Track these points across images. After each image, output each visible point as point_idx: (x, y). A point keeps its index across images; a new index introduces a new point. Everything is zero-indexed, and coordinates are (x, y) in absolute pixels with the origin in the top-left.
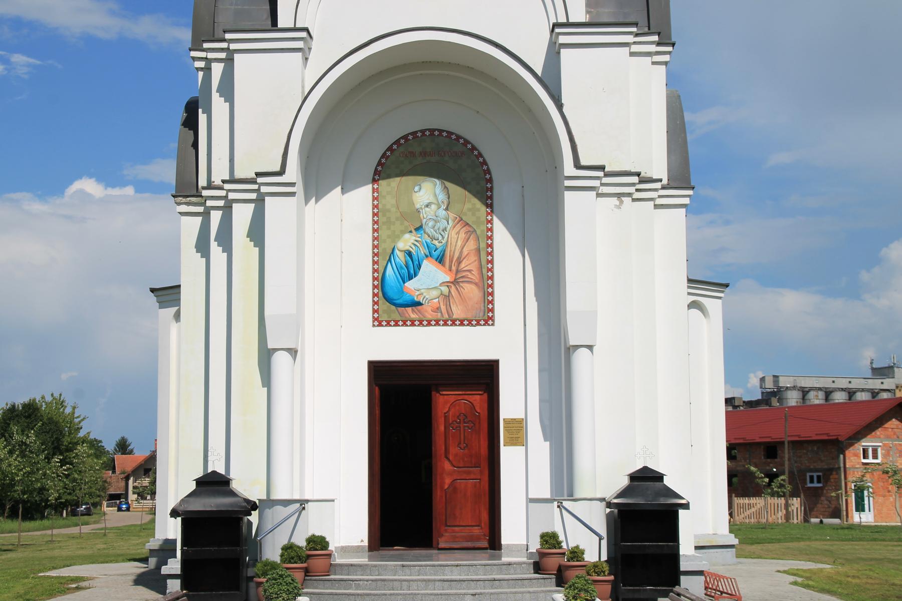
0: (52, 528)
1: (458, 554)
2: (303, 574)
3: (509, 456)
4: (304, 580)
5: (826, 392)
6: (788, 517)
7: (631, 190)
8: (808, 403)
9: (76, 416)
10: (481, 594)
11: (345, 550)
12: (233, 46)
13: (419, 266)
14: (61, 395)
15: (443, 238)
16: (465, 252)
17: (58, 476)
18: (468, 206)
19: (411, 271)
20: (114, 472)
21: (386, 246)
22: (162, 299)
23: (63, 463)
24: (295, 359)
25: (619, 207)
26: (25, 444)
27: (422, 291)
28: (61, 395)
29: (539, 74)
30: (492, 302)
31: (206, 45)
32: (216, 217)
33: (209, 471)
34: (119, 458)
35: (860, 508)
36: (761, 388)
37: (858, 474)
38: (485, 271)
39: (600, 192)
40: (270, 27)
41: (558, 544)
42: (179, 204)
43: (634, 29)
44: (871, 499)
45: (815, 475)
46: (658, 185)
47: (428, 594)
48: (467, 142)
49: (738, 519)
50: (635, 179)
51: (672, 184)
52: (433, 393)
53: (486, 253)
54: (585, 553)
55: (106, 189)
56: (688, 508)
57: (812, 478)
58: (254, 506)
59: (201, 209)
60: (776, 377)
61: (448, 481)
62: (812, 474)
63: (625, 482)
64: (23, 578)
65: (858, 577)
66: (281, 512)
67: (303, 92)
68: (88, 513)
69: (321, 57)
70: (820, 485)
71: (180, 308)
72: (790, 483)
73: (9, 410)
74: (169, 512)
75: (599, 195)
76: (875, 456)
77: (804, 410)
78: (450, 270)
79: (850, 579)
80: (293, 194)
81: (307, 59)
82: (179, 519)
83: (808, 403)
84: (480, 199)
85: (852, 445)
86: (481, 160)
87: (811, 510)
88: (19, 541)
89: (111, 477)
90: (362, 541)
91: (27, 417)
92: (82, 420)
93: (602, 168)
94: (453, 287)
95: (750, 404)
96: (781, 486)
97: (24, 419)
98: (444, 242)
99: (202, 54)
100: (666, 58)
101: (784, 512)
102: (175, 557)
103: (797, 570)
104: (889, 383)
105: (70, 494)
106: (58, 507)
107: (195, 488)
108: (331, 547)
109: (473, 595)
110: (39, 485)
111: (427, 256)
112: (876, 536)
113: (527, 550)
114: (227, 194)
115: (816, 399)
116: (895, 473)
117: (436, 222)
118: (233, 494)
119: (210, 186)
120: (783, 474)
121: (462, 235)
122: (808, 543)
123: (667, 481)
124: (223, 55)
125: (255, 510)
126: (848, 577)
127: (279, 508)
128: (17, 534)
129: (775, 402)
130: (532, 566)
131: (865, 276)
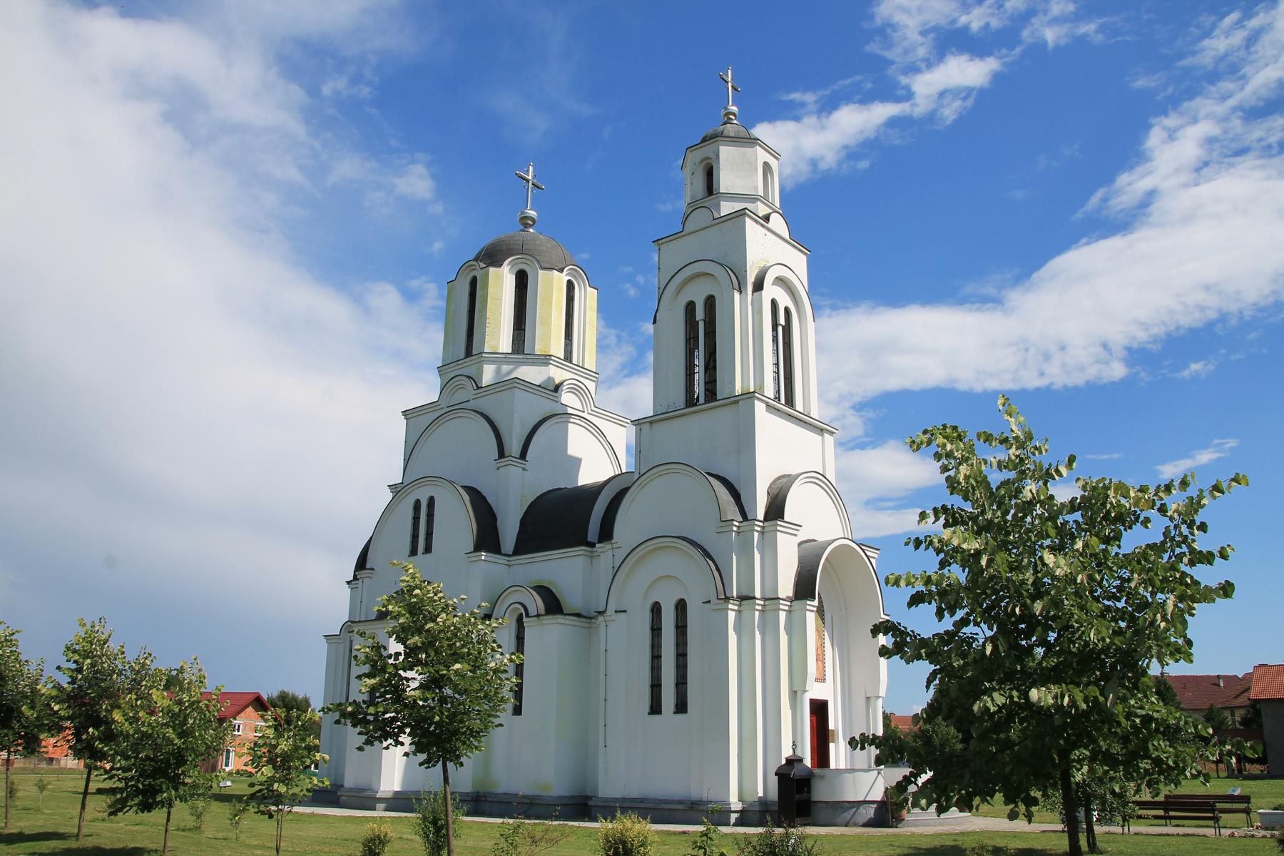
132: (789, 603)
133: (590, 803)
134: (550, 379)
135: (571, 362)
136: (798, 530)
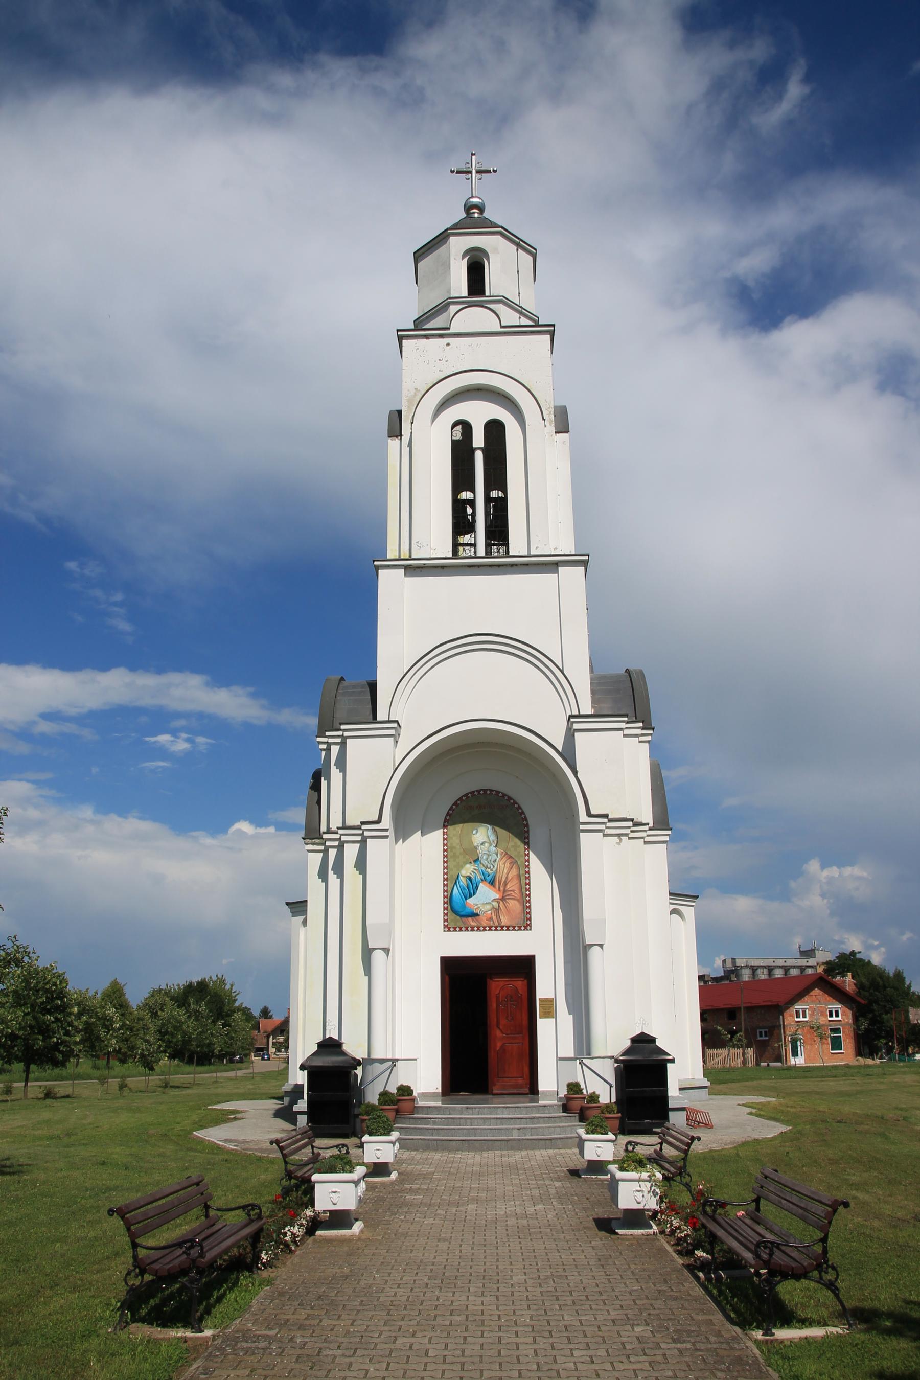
0: (217, 1072)
1: (507, 1098)
2: (395, 1113)
3: (544, 1026)
4: (396, 1118)
5: (769, 969)
6: (744, 1062)
7: (627, 831)
8: (757, 978)
9: (233, 991)
10: (524, 1128)
11: (425, 1095)
12: (346, 734)
13: (477, 888)
14: (223, 976)
15: (494, 867)
16: (510, 877)
17: (221, 1035)
18: (511, 844)
19: (471, 890)
20: (259, 1031)
21: (453, 873)
22: (294, 910)
23: (224, 1025)
24: (388, 956)
25: (619, 844)
26: (198, 1011)
27: (479, 905)
28: (223, 976)
29: (560, 750)
30: (529, 913)
31: (327, 734)
32: (332, 853)
33: (327, 1037)
34: (262, 1022)
35: (795, 1054)
36: (723, 967)
37: (793, 1030)
38: (524, 890)
39: (605, 833)
40: (371, 720)
41: (580, 1091)
42: (307, 844)
43: (626, 719)
44: (802, 1047)
45: (763, 1031)
46: (646, 828)
47: (485, 1129)
48: (510, 798)
49: (710, 1065)
50: (630, 824)
51: (656, 827)
52: (488, 980)
53: (524, 878)
54: (600, 1097)
55: (256, 828)
56: (674, 1062)
57: (761, 1033)
58: (358, 1063)
59: (322, 848)
60: (733, 959)
61: (499, 1045)
62: (760, 1030)
63: (628, 1044)
64: (197, 1109)
65: (795, 1107)
66: (379, 1068)
67: (394, 765)
68: (241, 1061)
69: (406, 742)
70: (767, 1038)
71: (306, 917)
72: (745, 1038)
73: (188, 986)
74: (299, 1066)
75: (604, 835)
76: (804, 1016)
77: (755, 983)
78: (499, 890)
79: (789, 1109)
80: (387, 837)
81: (397, 742)
82: (306, 1072)
83: (757, 978)
84: (520, 839)
85: (788, 1008)
86: (520, 811)
87: (761, 1057)
88: (194, 1081)
89: (257, 1035)
90: (437, 1089)
91: (199, 992)
92: (238, 994)
93: (606, 816)
94: (501, 902)
95: (716, 979)
96: (740, 1040)
97: (198, 993)
98: (494, 870)
99: (325, 740)
100: (649, 738)
101: (742, 1058)
102: (303, 1099)
103: (752, 1103)
104: (812, 962)
105: (228, 1047)
106: (221, 1057)
107: (317, 1049)
108: (415, 1094)
109: (518, 1129)
110: (208, 1041)
111: (482, 880)
112: (807, 1074)
113: (557, 1095)
114: (340, 837)
115: (762, 975)
116: (818, 1028)
117: (489, 855)
118: (344, 1054)
119: (329, 831)
120: (741, 1031)
121: (508, 865)
122: (759, 1082)
123: (658, 1043)
124: (339, 740)
125: (360, 1066)
126: (788, 1107)
127: (377, 1065)
128: (192, 1076)
129: (733, 978)
130: (561, 1107)
131: (793, 884)
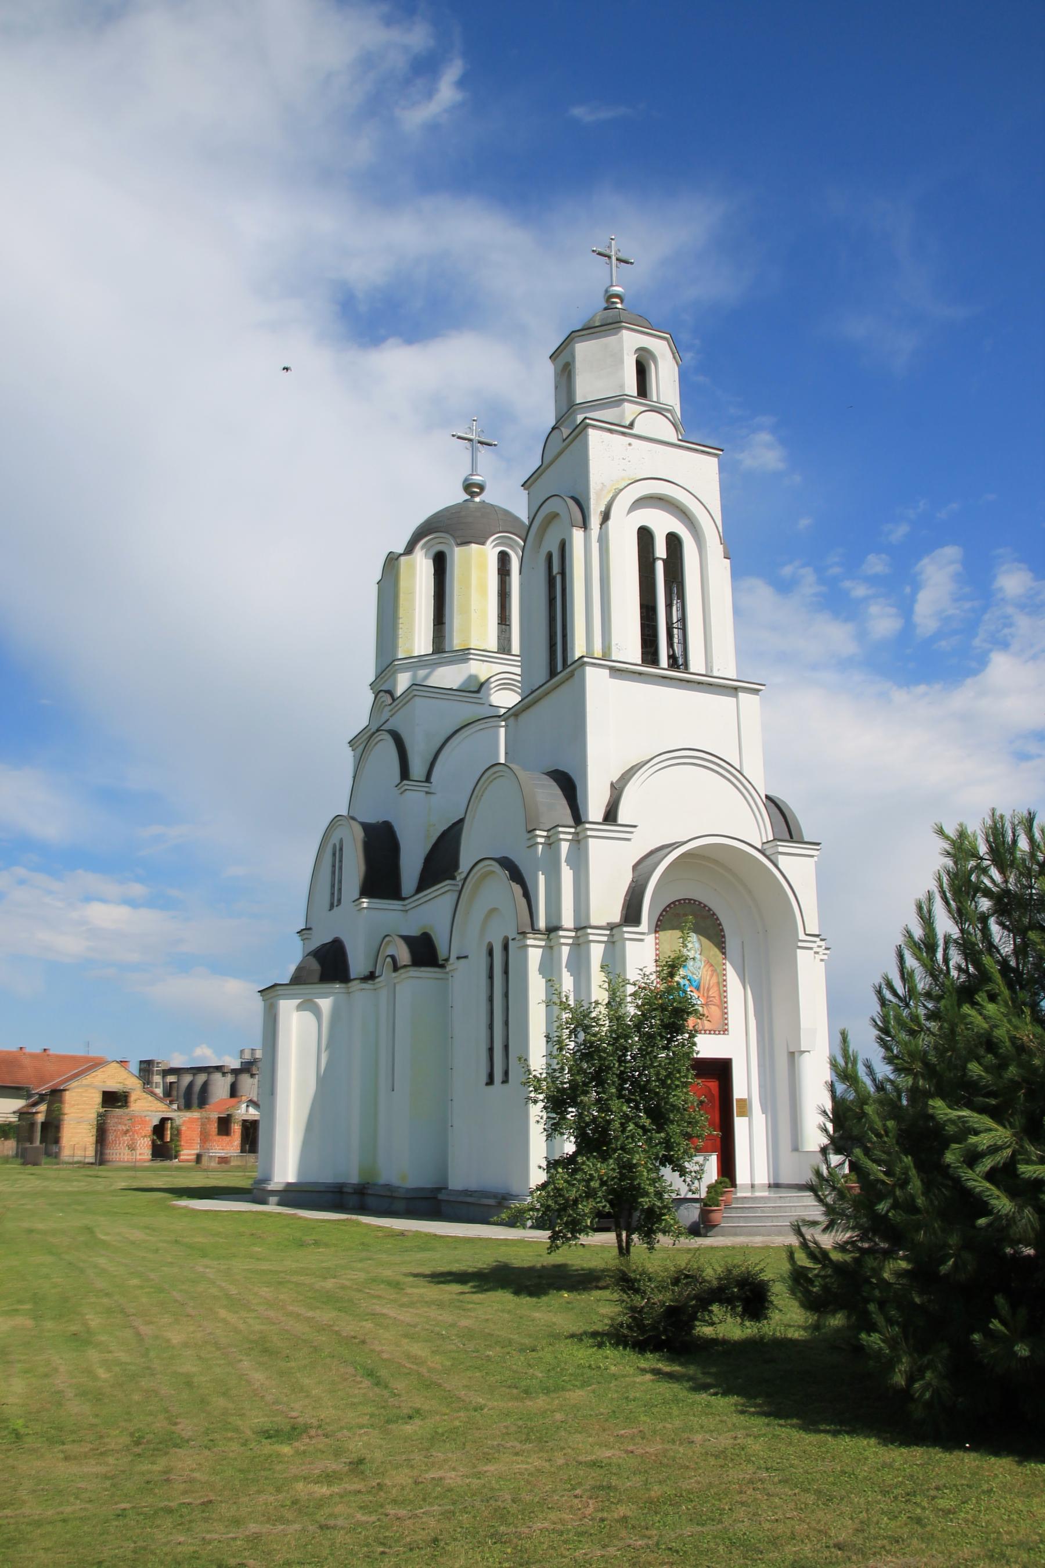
3: (740, 1124)
16: (711, 985)
18: (712, 953)
48: (710, 910)
53: (722, 984)
121: (709, 973)
132: (608, 932)
133: (440, 1197)
134: (472, 678)
135: (509, 653)
136: (631, 833)
